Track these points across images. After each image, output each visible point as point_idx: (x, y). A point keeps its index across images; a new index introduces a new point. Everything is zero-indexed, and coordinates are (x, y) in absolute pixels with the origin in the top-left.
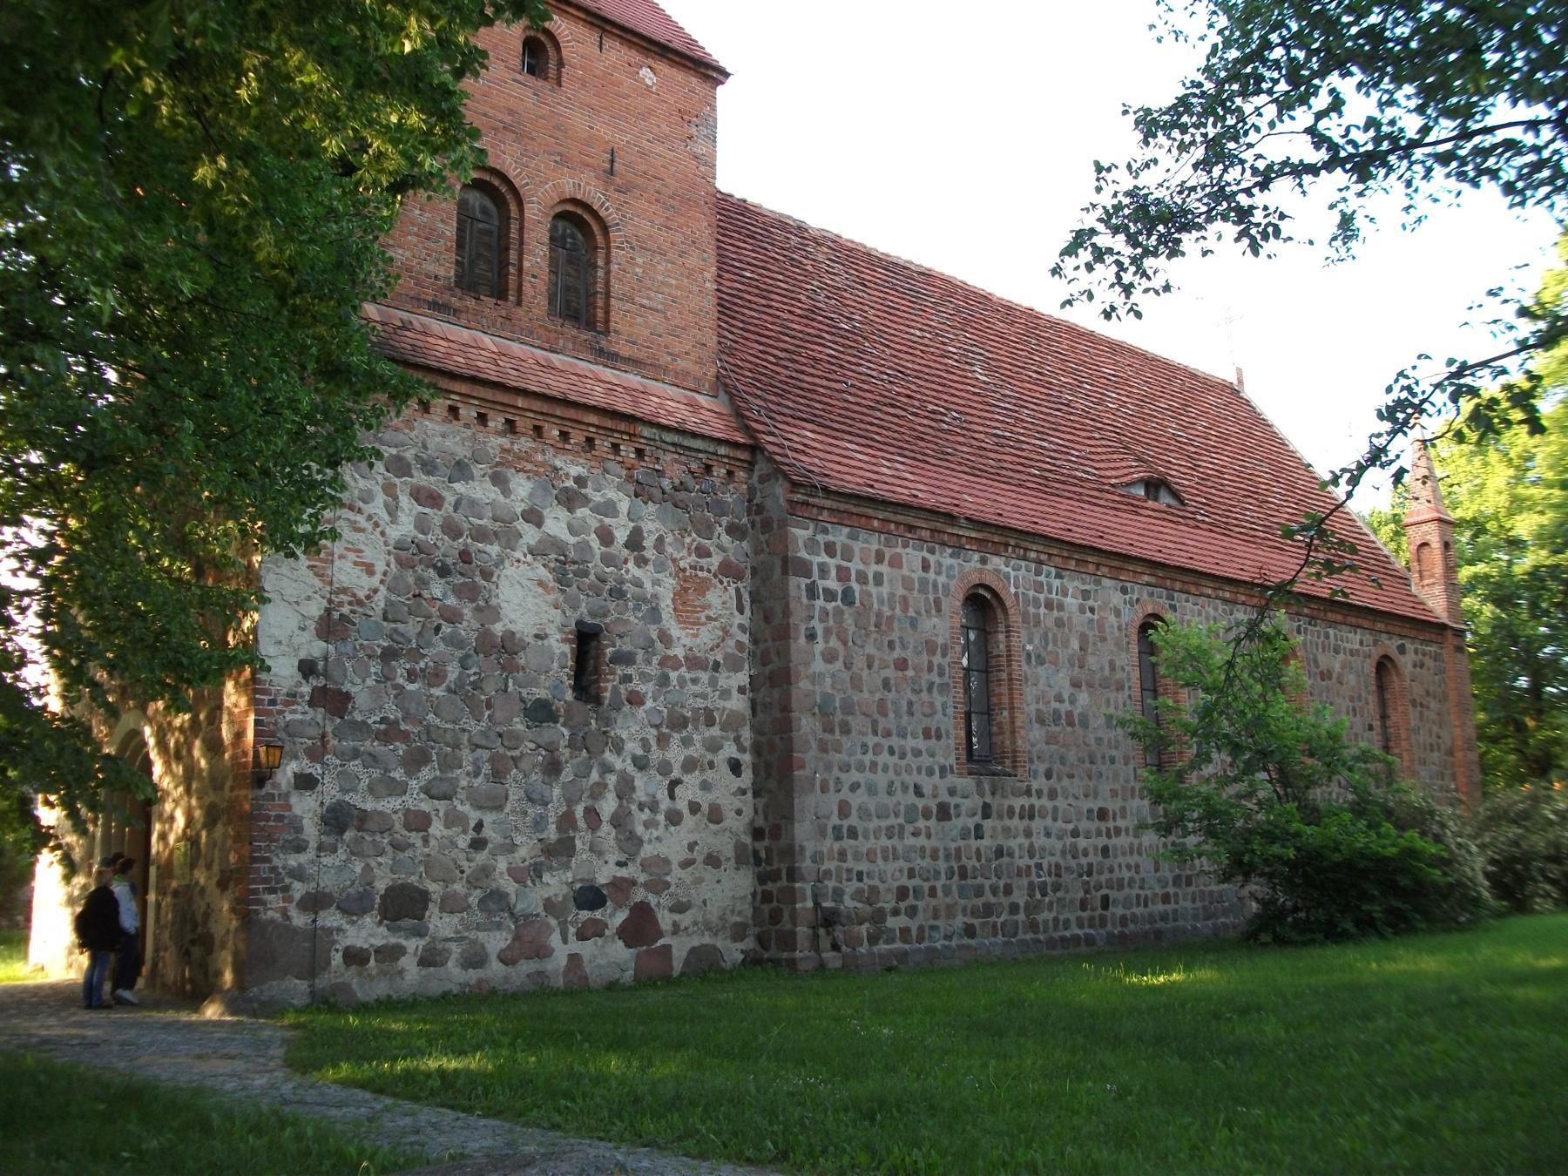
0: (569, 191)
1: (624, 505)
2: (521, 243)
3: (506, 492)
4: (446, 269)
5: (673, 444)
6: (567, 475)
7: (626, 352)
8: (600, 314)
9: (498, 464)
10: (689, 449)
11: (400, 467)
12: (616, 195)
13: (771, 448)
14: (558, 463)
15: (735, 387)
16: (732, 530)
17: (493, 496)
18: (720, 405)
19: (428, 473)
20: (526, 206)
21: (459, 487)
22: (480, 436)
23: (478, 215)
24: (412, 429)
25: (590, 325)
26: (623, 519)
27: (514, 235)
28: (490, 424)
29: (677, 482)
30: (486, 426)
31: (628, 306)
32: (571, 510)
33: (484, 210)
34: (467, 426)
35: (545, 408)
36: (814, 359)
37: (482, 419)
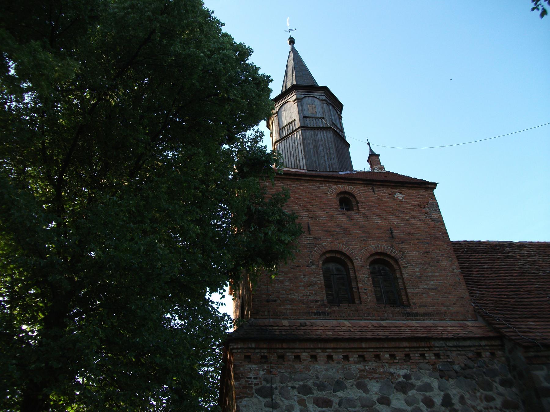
0: (373, 250)
1: (435, 384)
2: (356, 276)
3: (366, 391)
4: (321, 296)
5: (455, 347)
6: (399, 376)
7: (421, 311)
8: (404, 298)
9: (359, 378)
10: (464, 347)
11: (305, 390)
12: (398, 245)
13: (508, 334)
14: (392, 370)
15: (484, 312)
16: (503, 383)
17: (360, 395)
18: (480, 322)
19: (321, 390)
20: (354, 261)
21: (340, 394)
22: (347, 367)
23: (335, 272)
24: (309, 370)
25: (402, 304)
26: (436, 391)
27: (352, 275)
28: (351, 359)
29: (463, 365)
30: (349, 361)
31: (416, 291)
32: (405, 393)
33: (338, 270)
34: (338, 363)
35: (378, 345)
36: (528, 291)
37: (346, 358)
